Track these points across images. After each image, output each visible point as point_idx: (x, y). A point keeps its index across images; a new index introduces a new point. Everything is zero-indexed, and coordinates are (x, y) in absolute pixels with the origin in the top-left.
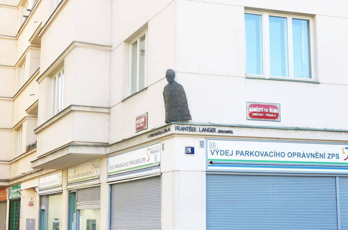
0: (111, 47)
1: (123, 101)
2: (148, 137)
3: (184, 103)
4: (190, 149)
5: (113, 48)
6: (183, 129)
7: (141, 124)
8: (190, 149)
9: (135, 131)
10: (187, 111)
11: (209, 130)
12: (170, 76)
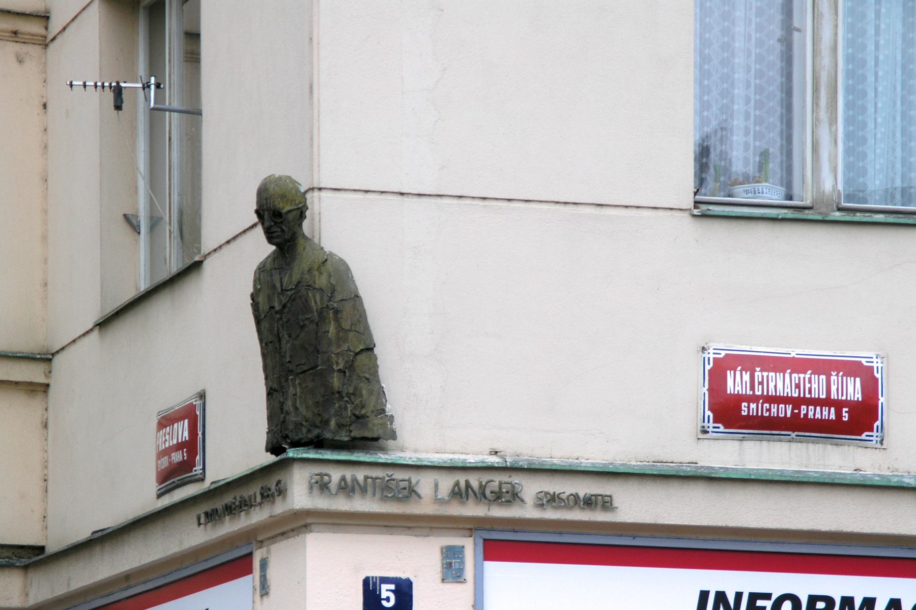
0: (45, 18)
1: (104, 324)
2: (199, 524)
3: (357, 354)
4: (392, 587)
5: (56, 25)
6: (347, 489)
7: (177, 450)
8: (392, 587)
9: (152, 486)
10: (371, 392)
11: (488, 493)
12: (281, 215)
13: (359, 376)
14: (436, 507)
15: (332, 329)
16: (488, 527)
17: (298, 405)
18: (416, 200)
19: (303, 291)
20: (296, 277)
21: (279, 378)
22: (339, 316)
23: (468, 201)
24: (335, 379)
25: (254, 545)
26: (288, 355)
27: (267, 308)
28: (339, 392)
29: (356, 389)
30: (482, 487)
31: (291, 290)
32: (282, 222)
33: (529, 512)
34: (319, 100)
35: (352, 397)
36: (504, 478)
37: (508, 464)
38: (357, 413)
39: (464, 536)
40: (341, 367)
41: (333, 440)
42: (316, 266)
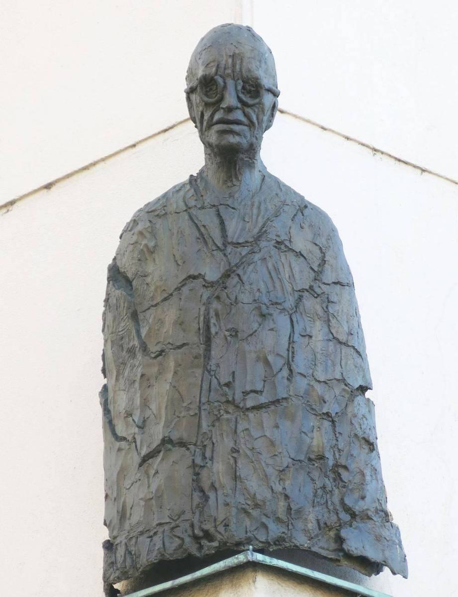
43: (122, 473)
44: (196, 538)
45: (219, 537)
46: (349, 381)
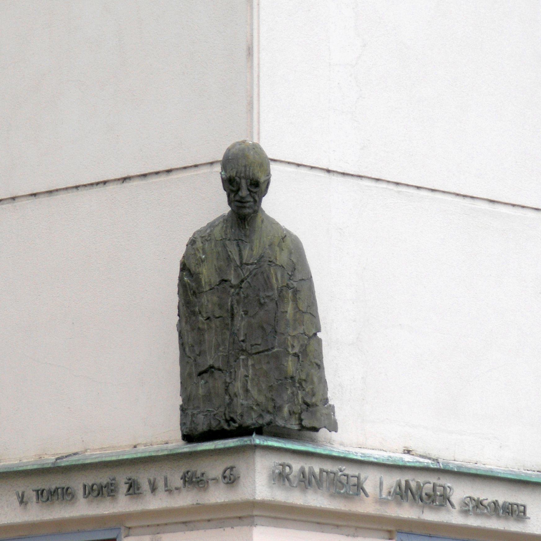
6: (307, 481)
13: (311, 362)
14: (378, 507)
15: (290, 308)
16: (407, 530)
17: (249, 388)
18: (341, 179)
19: (266, 265)
20: (257, 252)
21: (227, 357)
22: (298, 296)
23: (384, 185)
24: (290, 363)
25: (123, 532)
26: (242, 333)
27: (215, 279)
28: (292, 378)
29: (308, 375)
30: (419, 488)
31: (252, 264)
32: (256, 193)
33: (453, 517)
34: (259, 64)
35: (303, 383)
36: (433, 479)
37: (442, 467)
38: (308, 401)
39: (384, 538)
40: (296, 350)
41: (284, 427)
42: (276, 241)
43: (190, 375)
44: (227, 421)
45: (238, 421)
46: (307, 333)
